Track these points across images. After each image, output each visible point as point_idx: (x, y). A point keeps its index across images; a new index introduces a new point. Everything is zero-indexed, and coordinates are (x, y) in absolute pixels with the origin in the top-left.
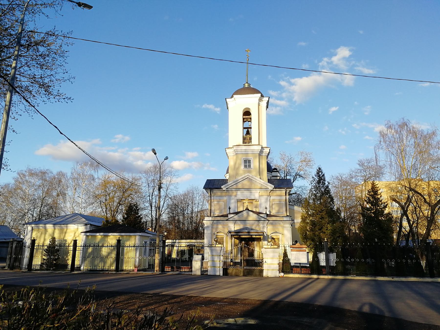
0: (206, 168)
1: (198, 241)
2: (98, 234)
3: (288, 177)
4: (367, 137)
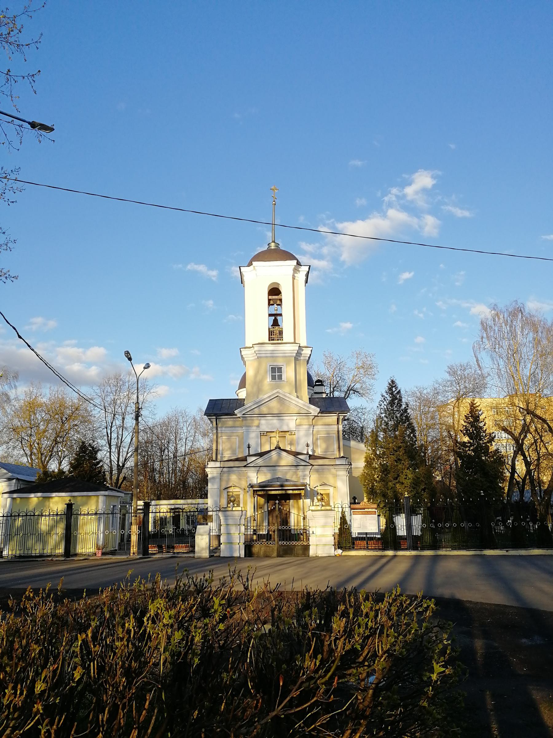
0: (192, 376)
1: (189, 501)
2: (32, 495)
3: (336, 394)
4: (459, 323)
